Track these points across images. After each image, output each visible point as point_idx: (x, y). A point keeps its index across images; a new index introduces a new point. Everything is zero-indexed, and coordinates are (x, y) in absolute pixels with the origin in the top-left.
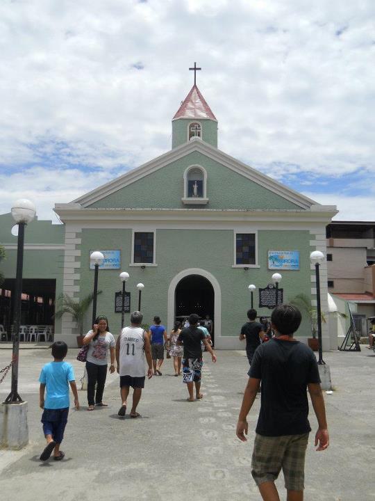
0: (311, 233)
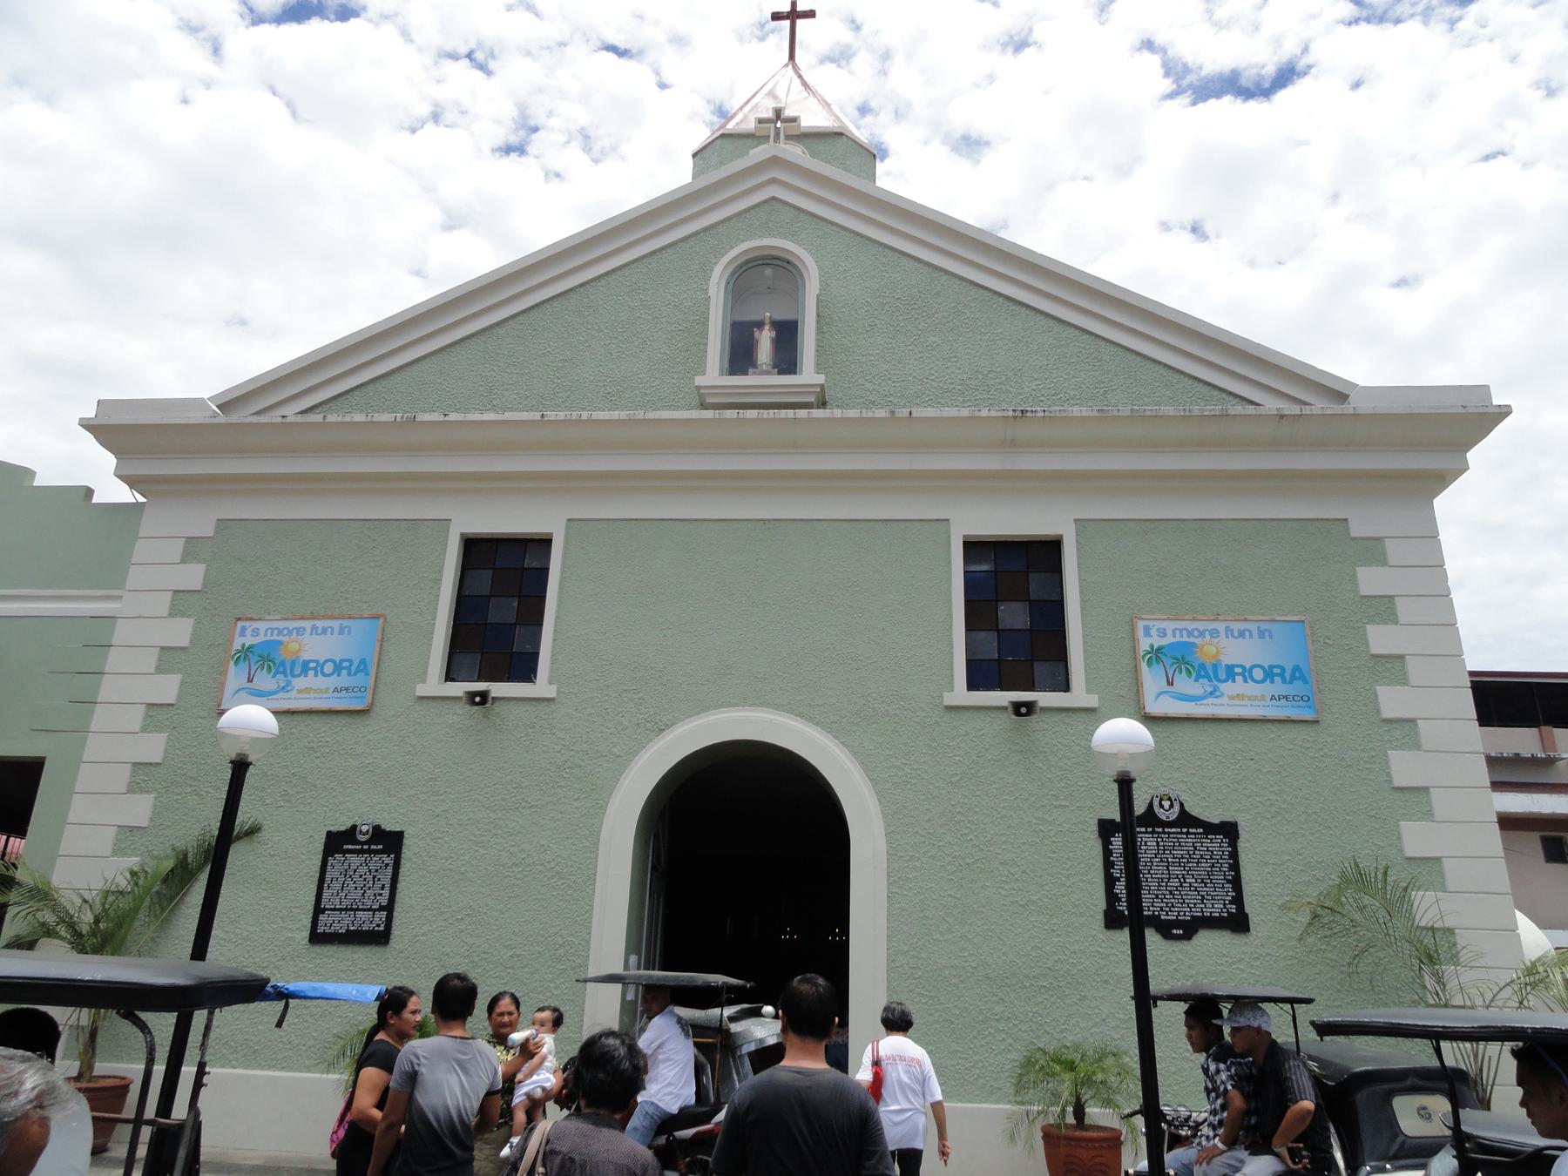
0: (1357, 530)
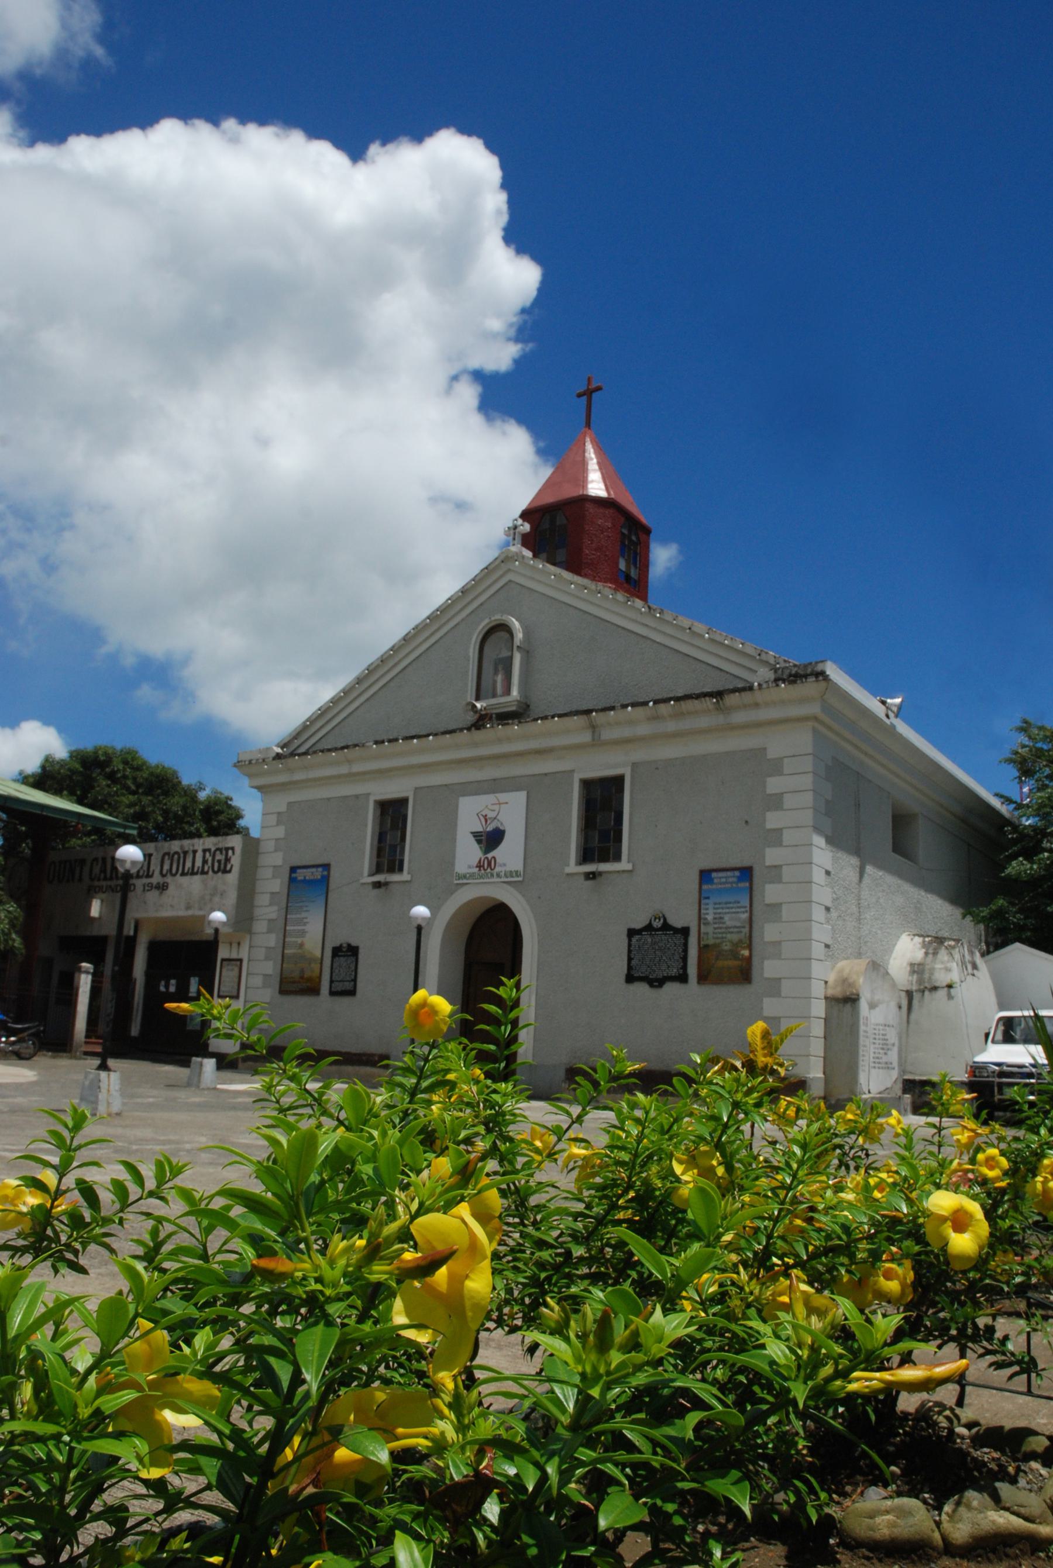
0: (771, 754)
